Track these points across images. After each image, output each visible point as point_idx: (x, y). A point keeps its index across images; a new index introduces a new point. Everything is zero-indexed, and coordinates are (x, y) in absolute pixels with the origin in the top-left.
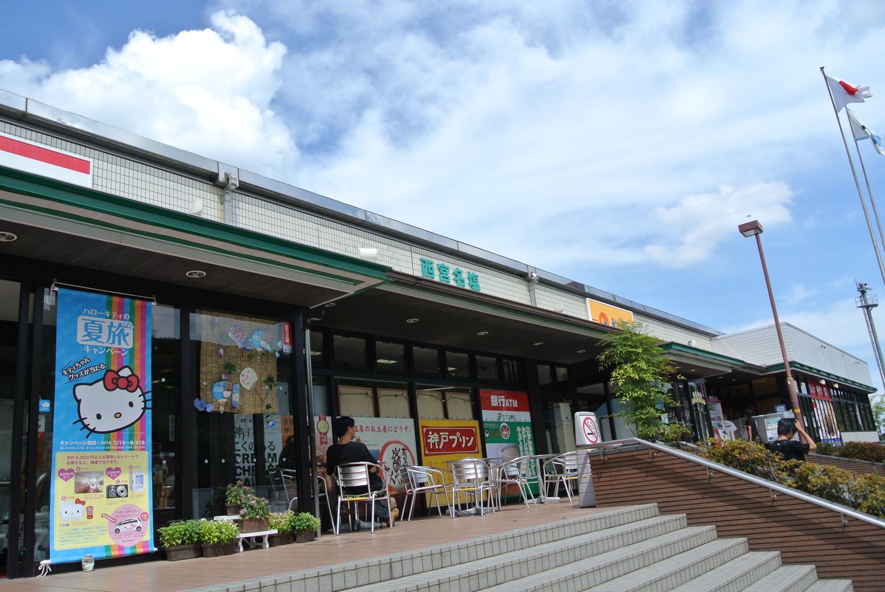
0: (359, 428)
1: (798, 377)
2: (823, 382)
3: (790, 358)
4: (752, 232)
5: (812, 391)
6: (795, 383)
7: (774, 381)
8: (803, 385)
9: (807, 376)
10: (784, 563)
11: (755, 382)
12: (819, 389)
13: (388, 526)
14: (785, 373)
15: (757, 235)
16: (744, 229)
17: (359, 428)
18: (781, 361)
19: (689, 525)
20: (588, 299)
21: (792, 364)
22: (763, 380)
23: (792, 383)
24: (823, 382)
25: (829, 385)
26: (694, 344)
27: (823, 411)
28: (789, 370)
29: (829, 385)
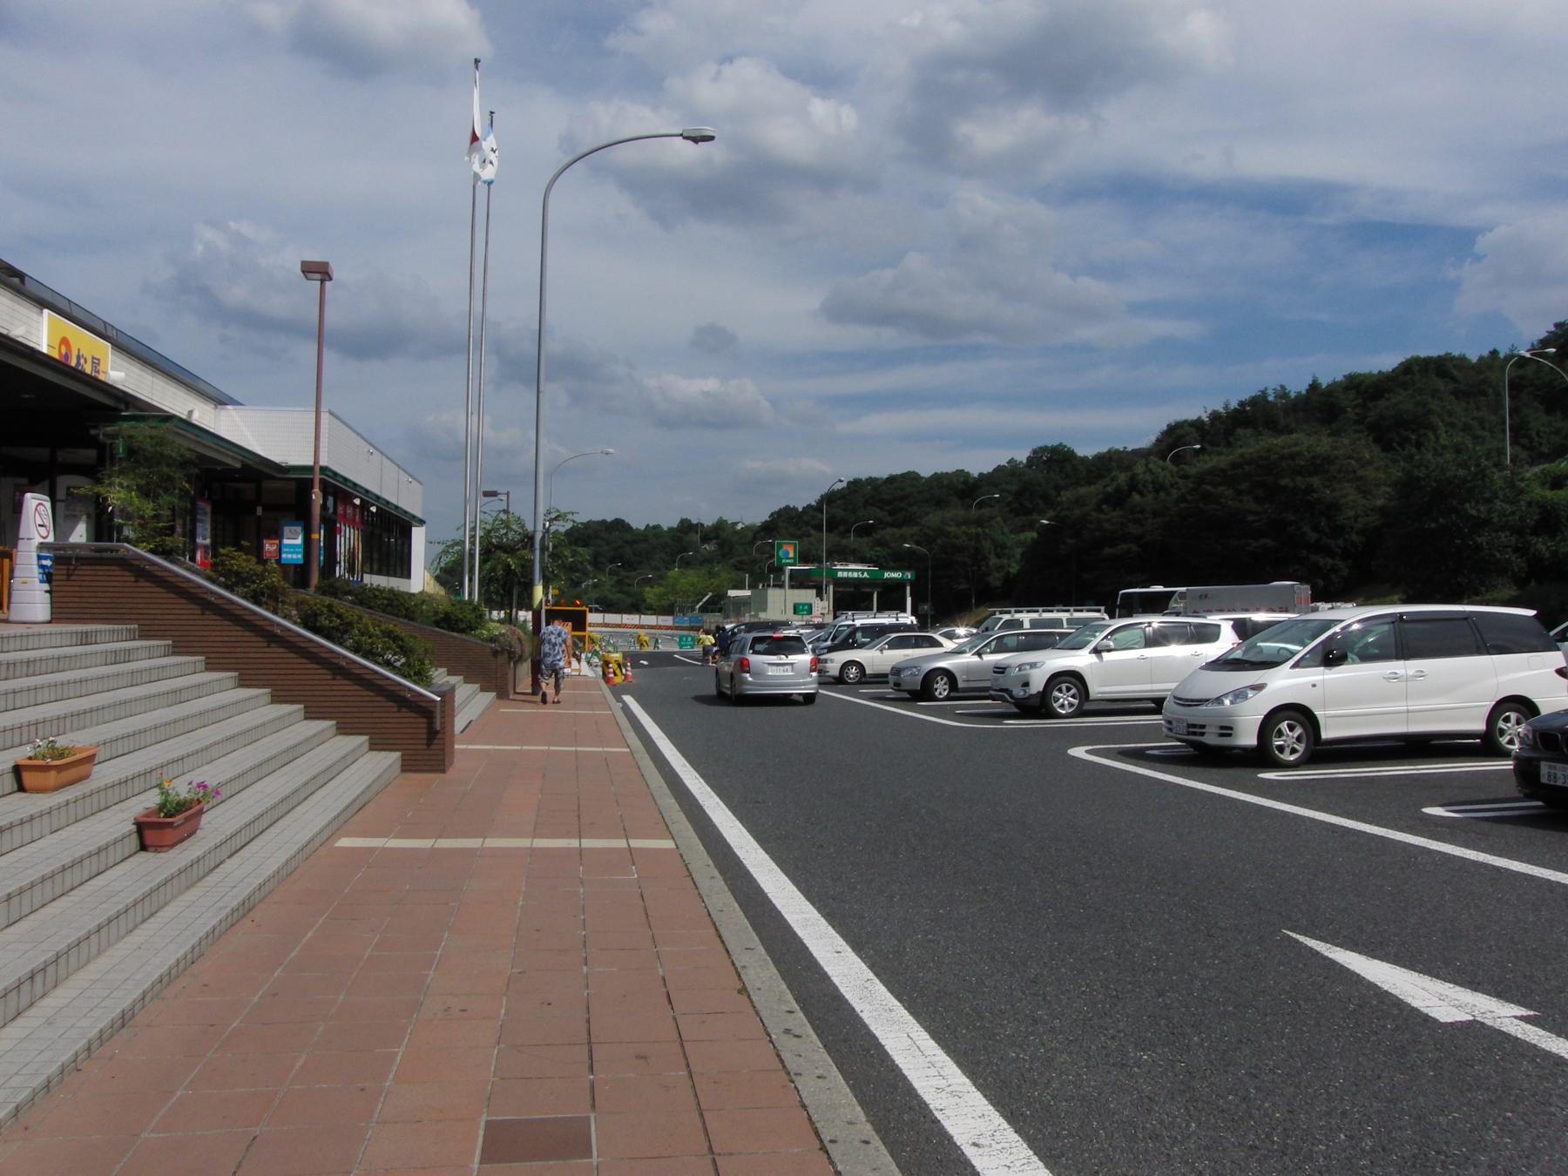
0: (496, 505)
1: (326, 488)
2: (357, 502)
3: (323, 462)
4: (318, 276)
5: (340, 509)
6: (320, 495)
7: (293, 486)
8: (331, 499)
9: (339, 489)
10: (306, 718)
11: (266, 484)
12: (350, 511)
13: (487, 553)
14: (312, 481)
15: (322, 281)
16: (309, 269)
17: (496, 505)
18: (311, 463)
19: (207, 669)
20: (46, 311)
21: (324, 469)
22: (279, 485)
23: (317, 496)
24: (357, 502)
25: (365, 505)
26: (196, 419)
27: (348, 539)
28: (317, 477)
29: (365, 505)
